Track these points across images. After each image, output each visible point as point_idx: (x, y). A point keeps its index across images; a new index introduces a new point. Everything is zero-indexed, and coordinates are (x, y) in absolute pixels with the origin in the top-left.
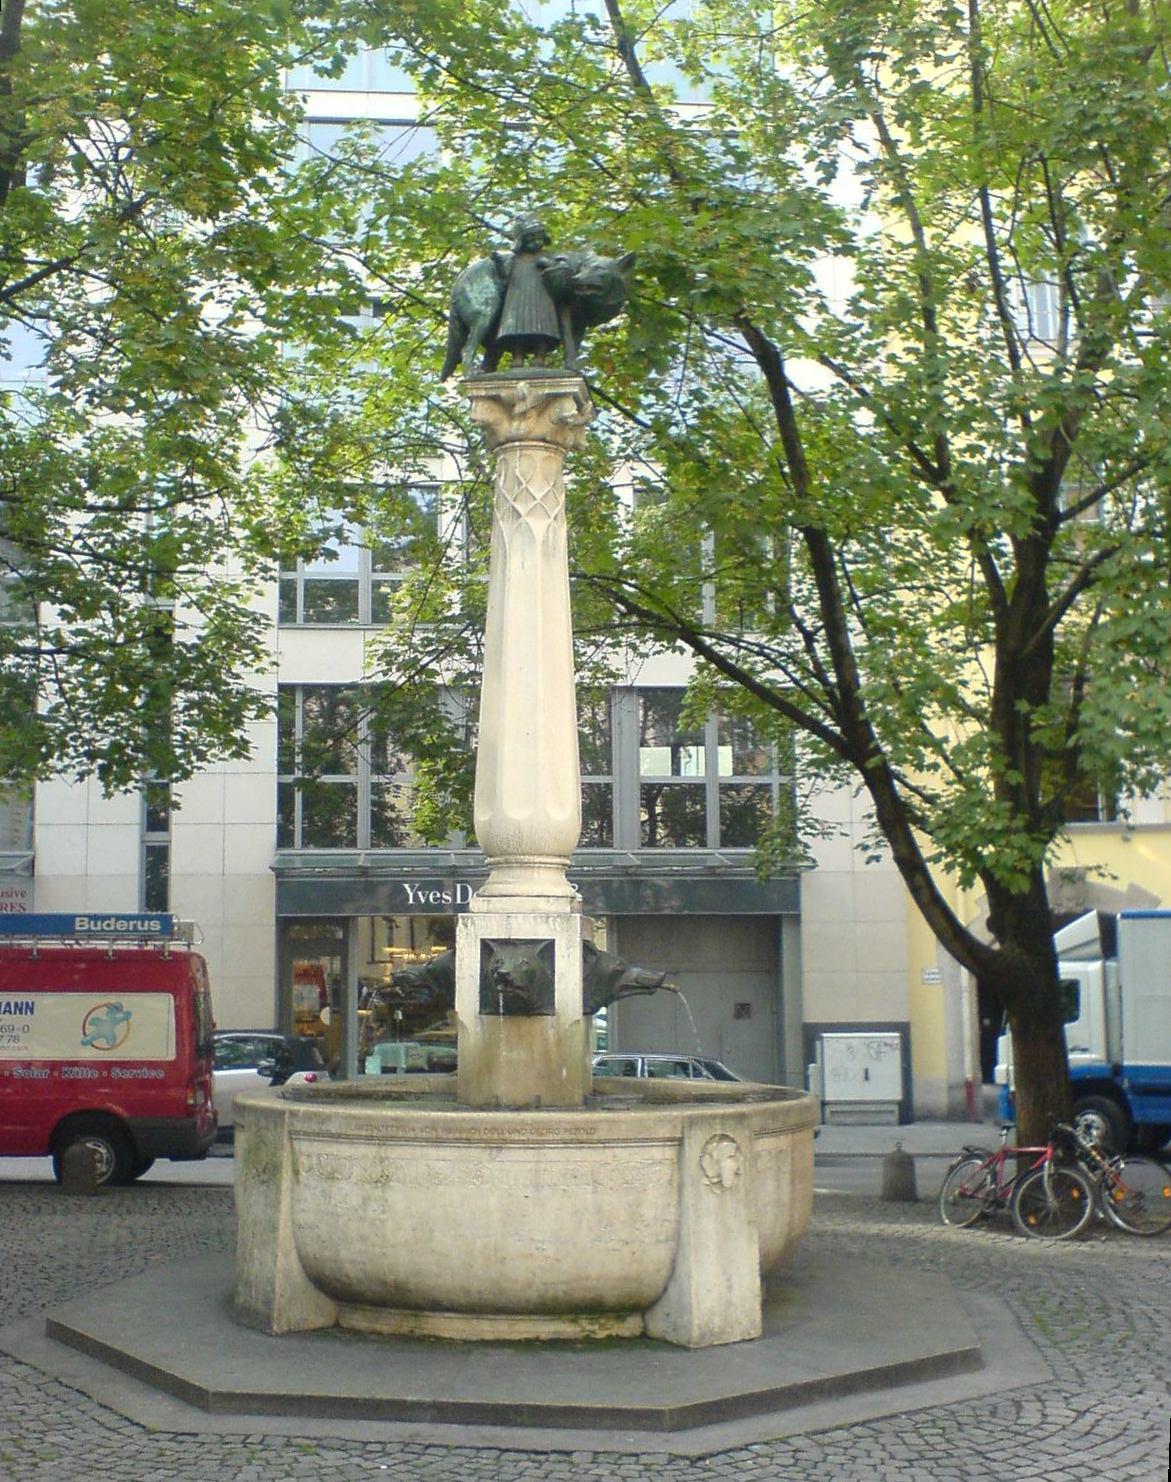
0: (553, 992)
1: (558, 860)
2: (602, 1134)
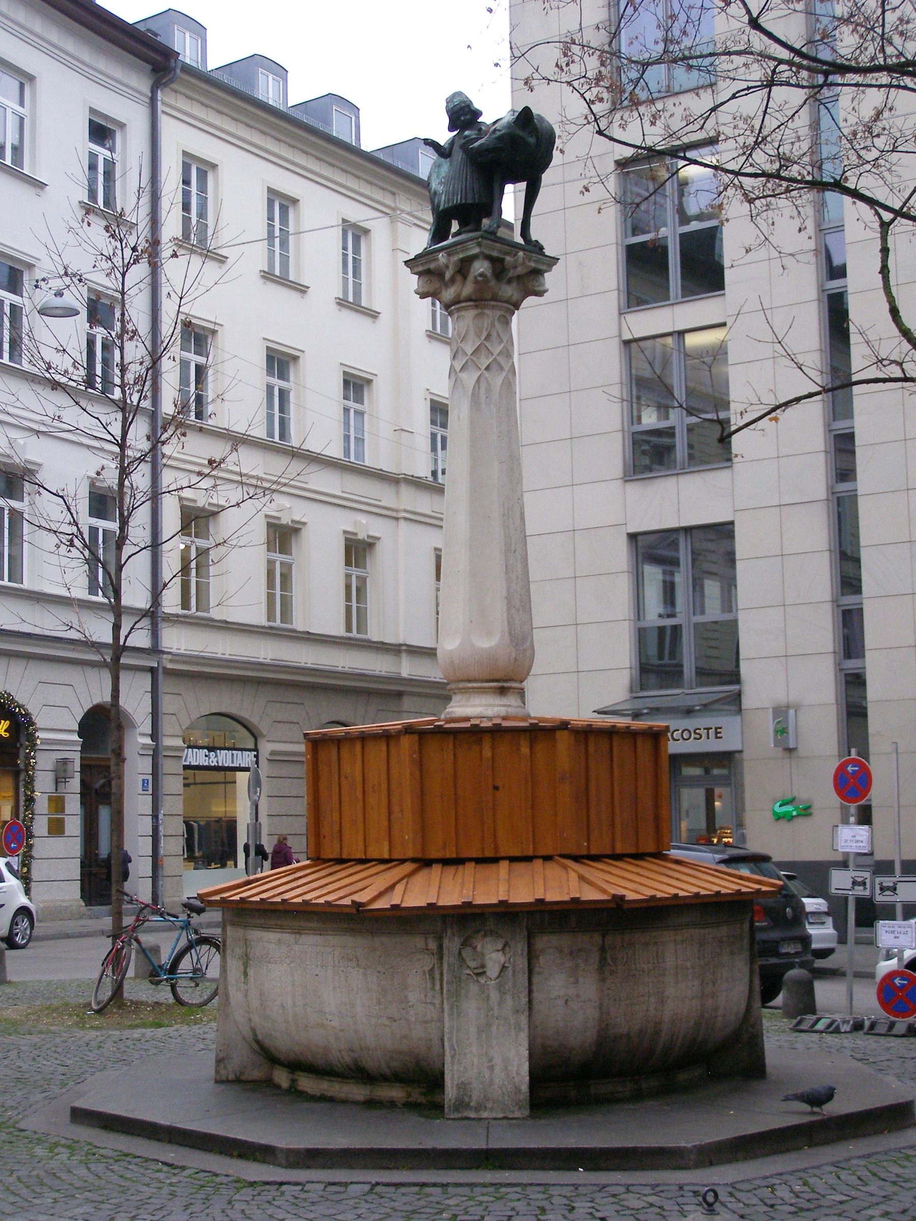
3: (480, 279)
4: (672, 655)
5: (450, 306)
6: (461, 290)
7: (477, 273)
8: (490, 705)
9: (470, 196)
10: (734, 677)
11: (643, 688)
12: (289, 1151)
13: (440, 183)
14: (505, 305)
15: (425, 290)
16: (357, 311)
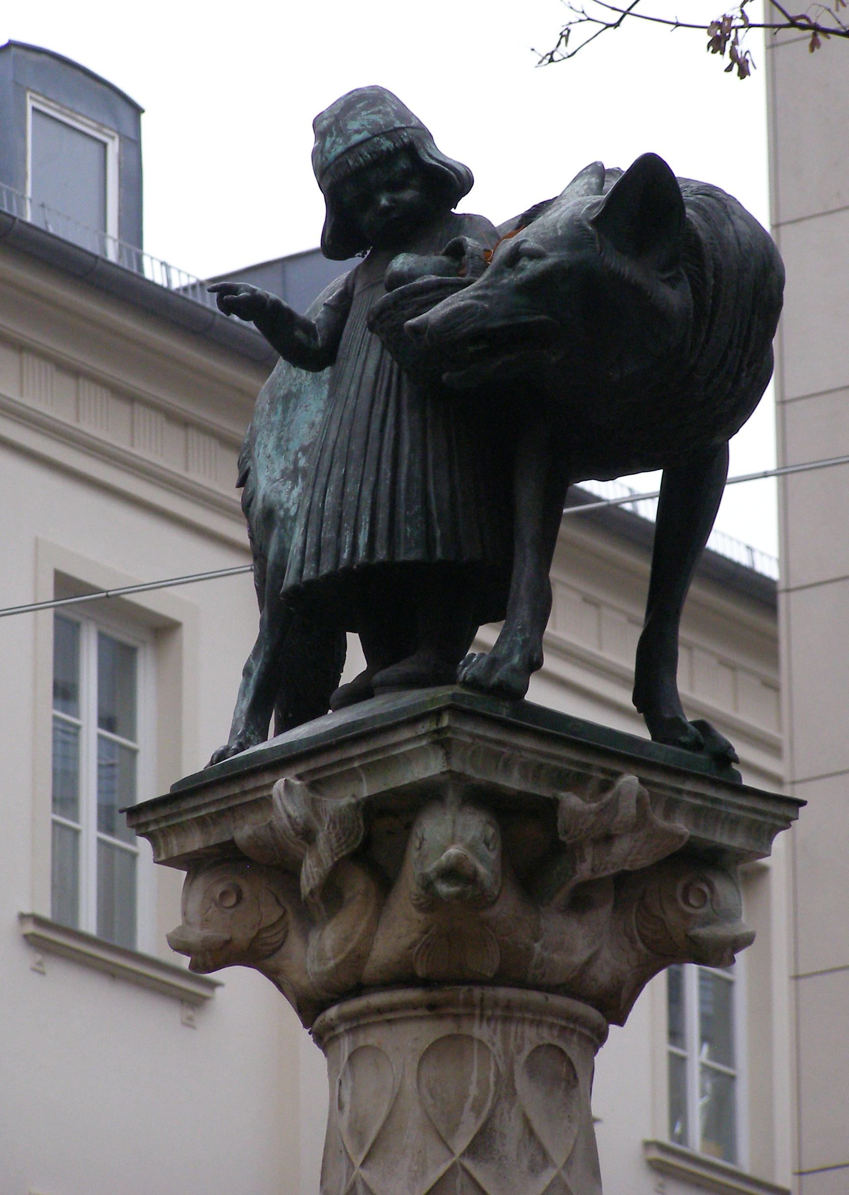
3: (444, 889)
5: (323, 1006)
6: (370, 934)
7: (431, 867)
13: (293, 474)
14: (559, 1001)
15: (216, 933)
16: (113, 973)
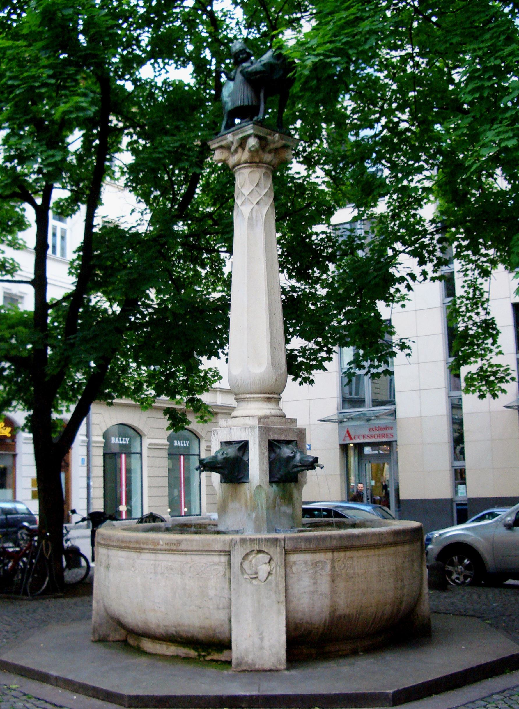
0: (248, 470)
1: (263, 395)
2: (182, 547)
4: (357, 393)
7: (250, 146)
8: (260, 409)
9: (246, 100)
10: (392, 402)
11: (343, 408)
12: (130, 697)
